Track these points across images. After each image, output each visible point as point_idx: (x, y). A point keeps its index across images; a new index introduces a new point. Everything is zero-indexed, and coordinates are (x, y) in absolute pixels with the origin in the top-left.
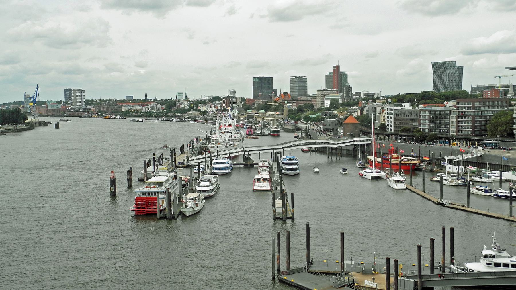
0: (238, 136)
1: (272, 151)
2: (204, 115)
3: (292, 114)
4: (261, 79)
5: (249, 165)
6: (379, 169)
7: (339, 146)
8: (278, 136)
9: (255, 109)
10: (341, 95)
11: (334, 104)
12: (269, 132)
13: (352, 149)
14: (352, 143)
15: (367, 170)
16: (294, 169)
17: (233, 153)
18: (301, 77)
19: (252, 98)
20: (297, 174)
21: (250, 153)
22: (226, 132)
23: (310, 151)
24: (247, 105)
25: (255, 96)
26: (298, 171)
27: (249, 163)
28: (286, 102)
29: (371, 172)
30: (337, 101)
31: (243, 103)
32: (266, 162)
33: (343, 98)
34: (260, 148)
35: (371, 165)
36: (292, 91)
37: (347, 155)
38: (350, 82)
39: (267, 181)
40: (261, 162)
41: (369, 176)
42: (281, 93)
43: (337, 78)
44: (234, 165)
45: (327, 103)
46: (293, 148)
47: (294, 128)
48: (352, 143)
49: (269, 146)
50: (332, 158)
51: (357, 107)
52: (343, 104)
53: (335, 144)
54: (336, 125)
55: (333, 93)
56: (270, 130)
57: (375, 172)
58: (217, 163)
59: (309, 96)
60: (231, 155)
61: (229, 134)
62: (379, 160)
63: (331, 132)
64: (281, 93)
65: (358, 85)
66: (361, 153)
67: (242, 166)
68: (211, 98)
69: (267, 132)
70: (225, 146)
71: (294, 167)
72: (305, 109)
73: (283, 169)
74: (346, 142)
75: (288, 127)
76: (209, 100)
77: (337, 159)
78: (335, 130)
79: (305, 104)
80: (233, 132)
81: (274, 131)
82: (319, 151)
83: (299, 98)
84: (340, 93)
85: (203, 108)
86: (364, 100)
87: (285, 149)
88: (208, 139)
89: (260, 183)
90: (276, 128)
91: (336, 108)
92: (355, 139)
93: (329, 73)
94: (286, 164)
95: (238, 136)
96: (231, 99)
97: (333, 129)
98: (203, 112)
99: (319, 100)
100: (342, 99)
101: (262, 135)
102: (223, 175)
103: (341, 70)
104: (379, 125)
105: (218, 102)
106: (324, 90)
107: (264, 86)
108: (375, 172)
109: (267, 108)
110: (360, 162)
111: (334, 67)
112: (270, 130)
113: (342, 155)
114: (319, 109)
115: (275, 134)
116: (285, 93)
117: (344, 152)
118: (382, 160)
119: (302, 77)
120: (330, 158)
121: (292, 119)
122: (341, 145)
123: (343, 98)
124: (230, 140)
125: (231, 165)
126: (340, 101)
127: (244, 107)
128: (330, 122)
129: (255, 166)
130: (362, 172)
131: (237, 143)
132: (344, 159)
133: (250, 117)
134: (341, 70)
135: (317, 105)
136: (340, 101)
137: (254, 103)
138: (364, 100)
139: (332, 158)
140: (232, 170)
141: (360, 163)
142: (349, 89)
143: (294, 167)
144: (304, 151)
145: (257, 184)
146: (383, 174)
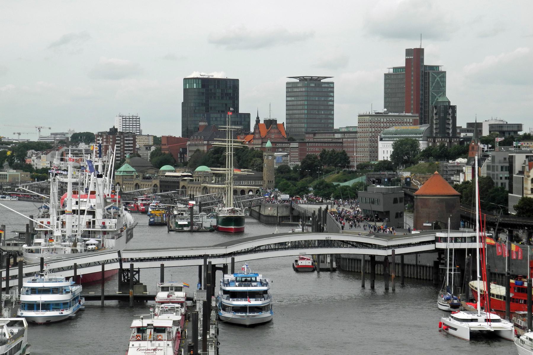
0: (111, 223)
1: (201, 262)
2: (40, 179)
3: (286, 179)
4: (207, 83)
5: (133, 298)
6: (497, 312)
7: (394, 255)
8: (240, 232)
9: (185, 164)
10: (424, 128)
11: (405, 153)
12: (214, 222)
13: (430, 264)
14: (431, 247)
15: (462, 315)
16: (253, 309)
17: (88, 265)
18: (316, 81)
19: (177, 133)
20: (265, 324)
21: (136, 265)
22: (74, 212)
23: (317, 266)
24: (166, 152)
25: (187, 132)
26: (265, 315)
27: (132, 293)
28: (269, 144)
29: (467, 322)
30: (414, 145)
31: (153, 148)
32: (179, 289)
33: (429, 136)
34: (169, 261)
35: (473, 300)
36: (289, 117)
37: (418, 281)
38: (453, 94)
39: (164, 336)
40: (164, 289)
41: (463, 330)
42: (258, 121)
43: (417, 85)
44: (88, 298)
45: (385, 151)
46: (271, 263)
47: (285, 212)
48: (431, 247)
49: (192, 248)
50: (373, 287)
51: (465, 160)
52: (427, 154)
53: (381, 246)
54: (395, 201)
55: (402, 123)
56: (217, 217)
57: (483, 321)
58: (34, 291)
59: (338, 132)
60: (81, 272)
61: (87, 218)
62: (499, 290)
63: (381, 220)
64: (258, 121)
65: (472, 103)
66: (450, 272)
67: (114, 303)
68: (70, 136)
69: (208, 222)
70: (69, 250)
71: (253, 302)
72: (325, 167)
73: (224, 308)
74: (412, 242)
75: (268, 211)
76: (63, 143)
77: (387, 289)
78: (392, 215)
79: (324, 153)
80: (99, 213)
81: (227, 220)
82: (345, 267)
83: (309, 138)
84: (422, 122)
85: (39, 162)
86: (485, 141)
87: (237, 258)
88: (29, 234)
89: (144, 339)
90: (233, 211)
91: (408, 163)
92: (439, 235)
93: (395, 69)
94: (234, 295)
95: (111, 223)
96: (121, 140)
97: (387, 213)
98: (37, 171)
99: (363, 143)
100: (426, 138)
101: (194, 229)
102: (49, 323)
103: (428, 61)
104: (516, 204)
105: (82, 146)
106: (378, 115)
107: (212, 103)
108: (483, 321)
109: (216, 158)
110: (448, 295)
111: (409, 52)
112: (217, 217)
113: (404, 280)
114: (363, 167)
115: (231, 226)
116: (271, 123)
117: (409, 272)
118: (508, 292)
119: (318, 79)
120: (368, 285)
121: (283, 190)
122: (398, 251)
123: (429, 136)
124: (88, 234)
125: (75, 299)
126: (423, 145)
127: (155, 159)
128: (379, 191)
129: (150, 302)
130: (447, 321)
131: (110, 243)
132: (412, 290)
133: (168, 185)
134: (428, 61)
135: (359, 157)
136: (423, 145)
137: (185, 151)
138: (485, 141)
139: (373, 287)
140: (79, 312)
141: (448, 299)
142: (447, 113)
143: (253, 302)
144: (299, 269)
145: (136, 344)
146: (505, 326)
